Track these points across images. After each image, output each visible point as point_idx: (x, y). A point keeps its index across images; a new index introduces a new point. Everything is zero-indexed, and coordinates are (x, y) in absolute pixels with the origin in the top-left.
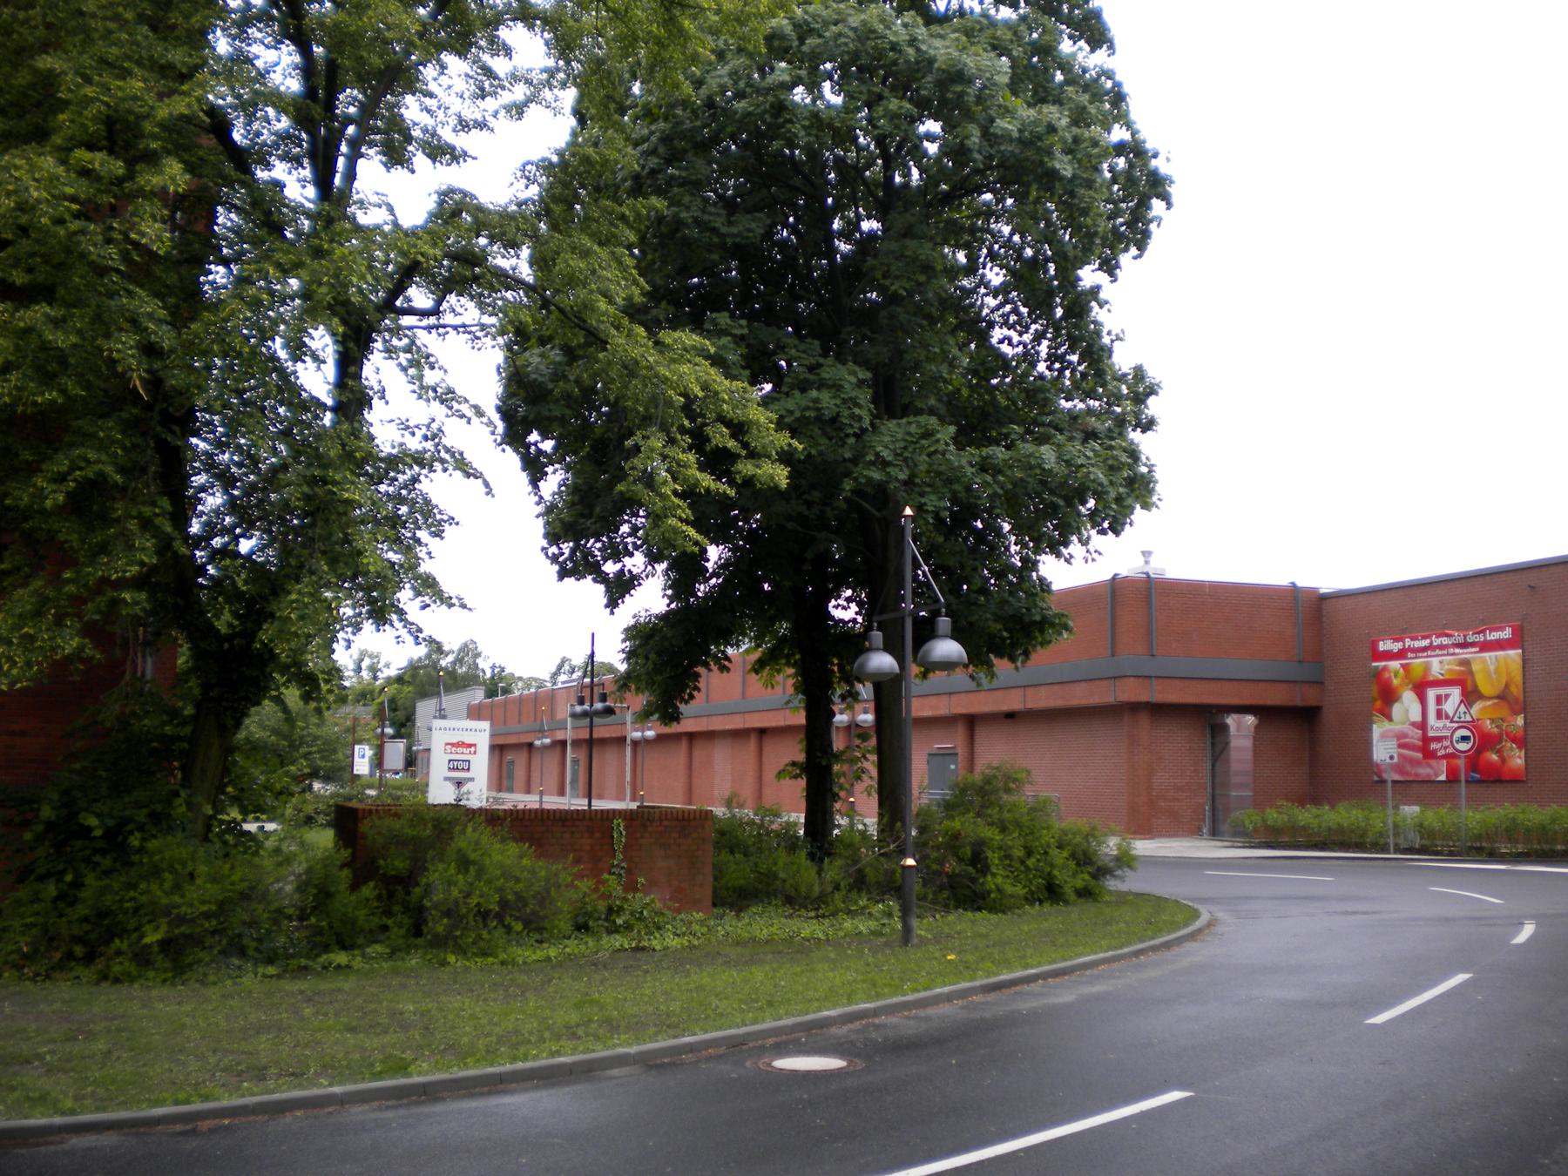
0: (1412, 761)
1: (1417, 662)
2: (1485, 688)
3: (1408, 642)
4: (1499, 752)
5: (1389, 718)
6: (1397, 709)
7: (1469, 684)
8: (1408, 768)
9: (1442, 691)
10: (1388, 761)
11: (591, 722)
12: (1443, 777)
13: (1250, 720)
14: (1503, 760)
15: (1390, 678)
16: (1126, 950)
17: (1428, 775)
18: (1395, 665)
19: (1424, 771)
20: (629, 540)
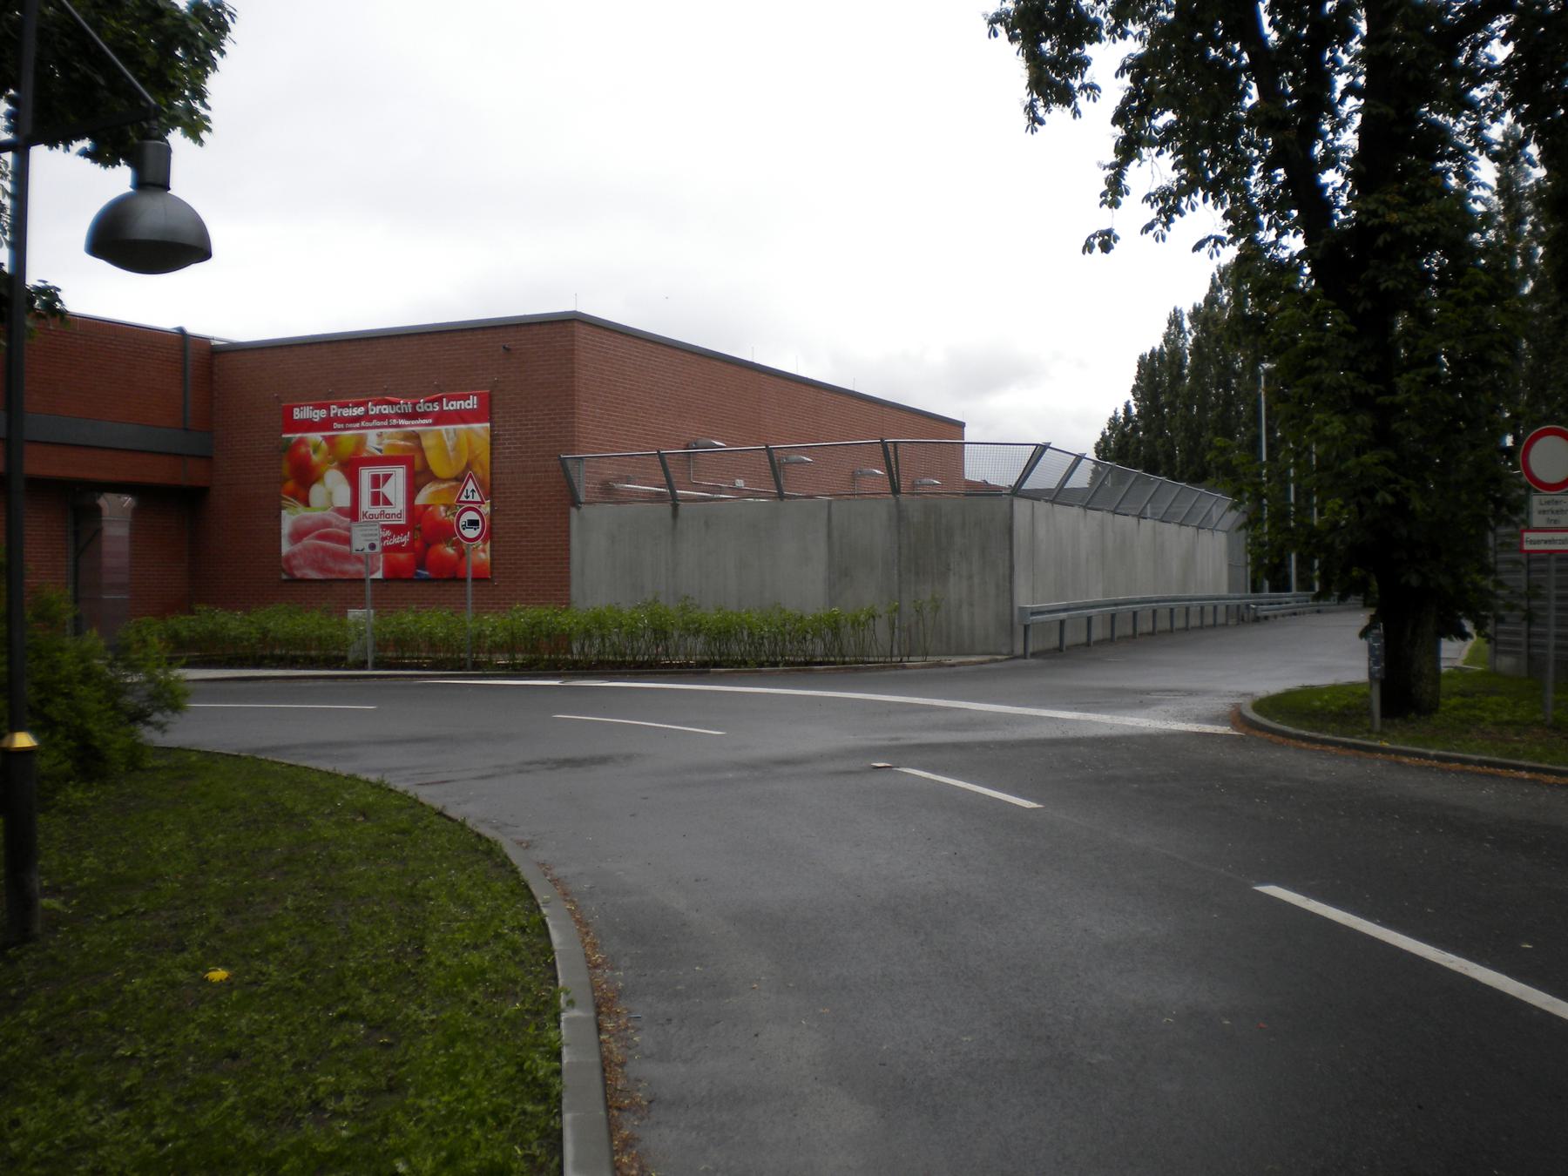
1: (347, 435)
3: (334, 410)
5: (307, 503)
6: (316, 493)
8: (331, 564)
9: (381, 471)
10: (367, 550)
13: (128, 501)
15: (308, 452)
17: (359, 572)
18: (315, 437)
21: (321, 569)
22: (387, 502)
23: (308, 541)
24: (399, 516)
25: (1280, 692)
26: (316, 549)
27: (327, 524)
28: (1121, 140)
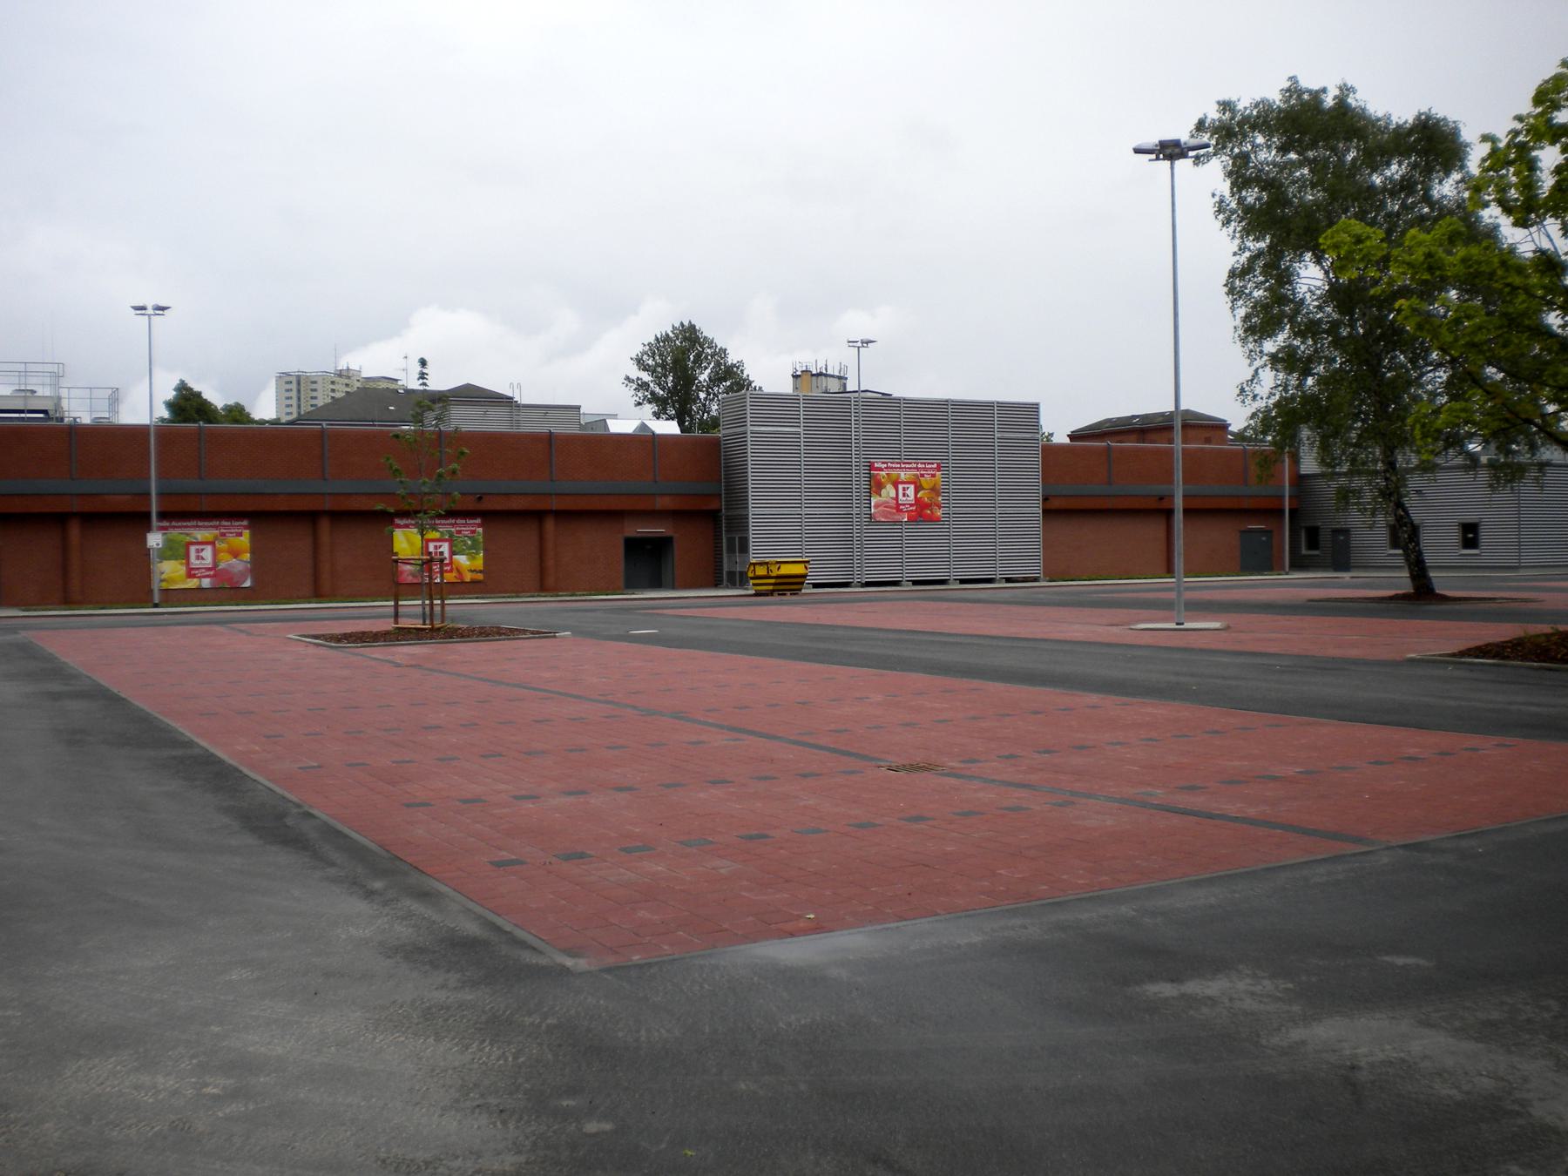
0: (890, 513)
1: (894, 473)
2: (925, 485)
4: (931, 510)
5: (880, 495)
6: (883, 492)
7: (918, 484)
9: (906, 486)
11: (396, 606)
12: (906, 520)
14: (932, 512)
16: (1172, 882)
19: (897, 517)
20: (420, 522)
21: (886, 517)
22: (203, 559)
23: (880, 508)
24: (208, 564)
25: (776, 941)
26: (884, 511)
27: (888, 503)
28: (834, 386)
